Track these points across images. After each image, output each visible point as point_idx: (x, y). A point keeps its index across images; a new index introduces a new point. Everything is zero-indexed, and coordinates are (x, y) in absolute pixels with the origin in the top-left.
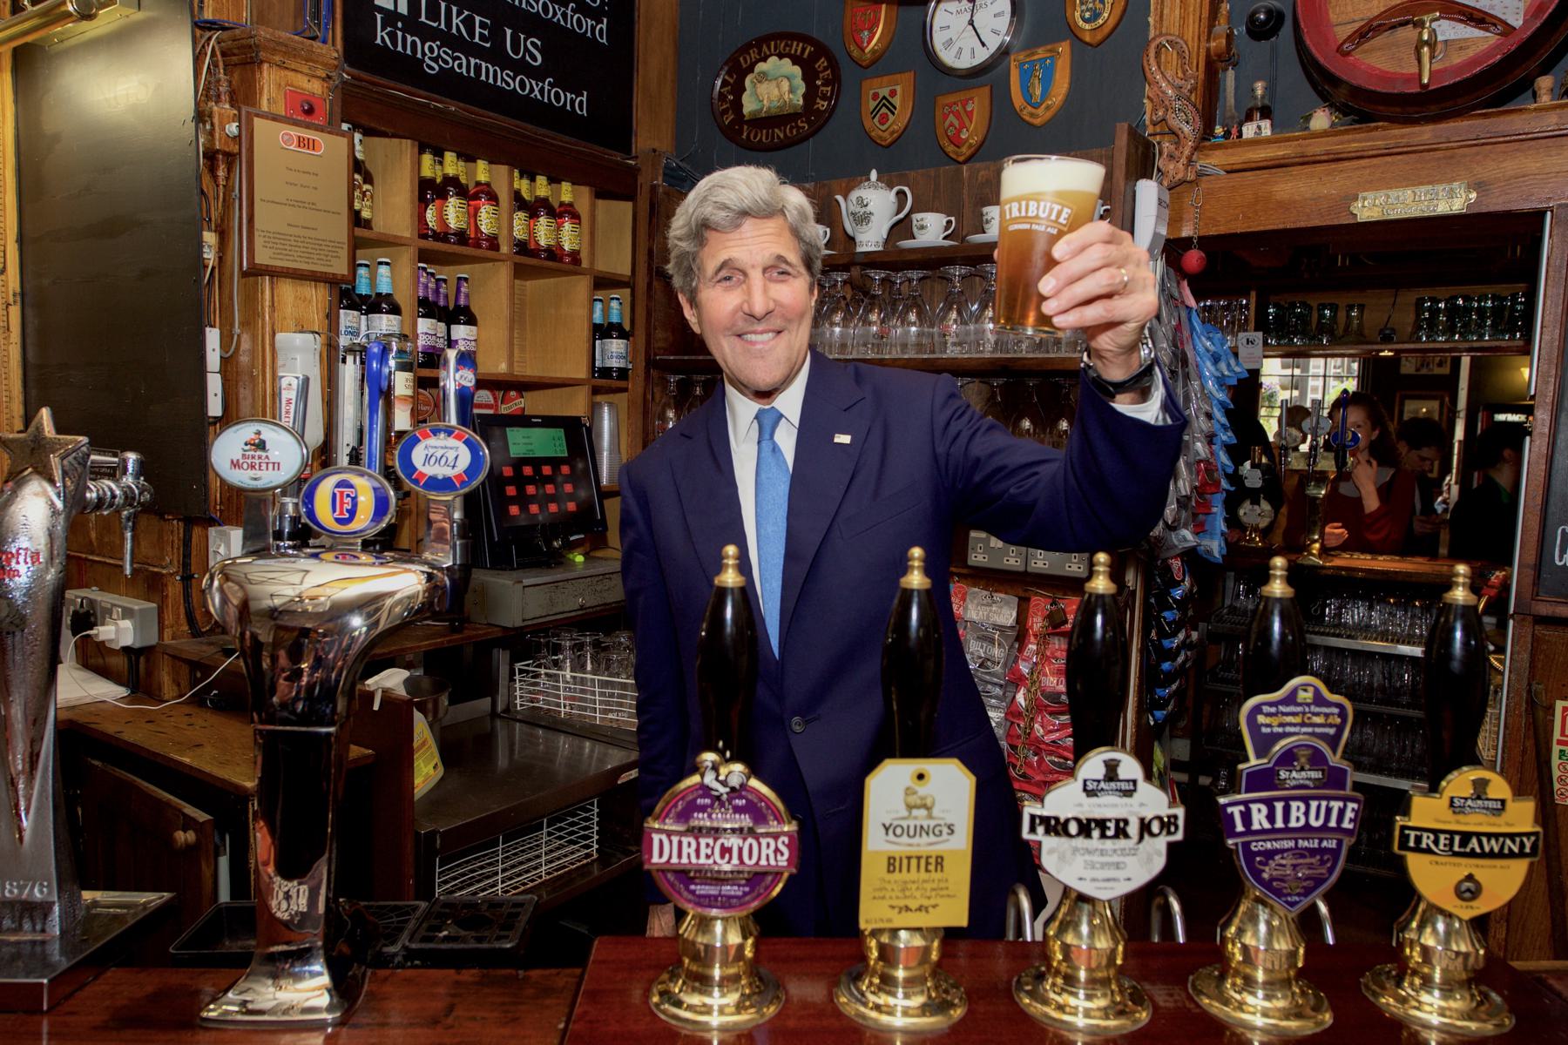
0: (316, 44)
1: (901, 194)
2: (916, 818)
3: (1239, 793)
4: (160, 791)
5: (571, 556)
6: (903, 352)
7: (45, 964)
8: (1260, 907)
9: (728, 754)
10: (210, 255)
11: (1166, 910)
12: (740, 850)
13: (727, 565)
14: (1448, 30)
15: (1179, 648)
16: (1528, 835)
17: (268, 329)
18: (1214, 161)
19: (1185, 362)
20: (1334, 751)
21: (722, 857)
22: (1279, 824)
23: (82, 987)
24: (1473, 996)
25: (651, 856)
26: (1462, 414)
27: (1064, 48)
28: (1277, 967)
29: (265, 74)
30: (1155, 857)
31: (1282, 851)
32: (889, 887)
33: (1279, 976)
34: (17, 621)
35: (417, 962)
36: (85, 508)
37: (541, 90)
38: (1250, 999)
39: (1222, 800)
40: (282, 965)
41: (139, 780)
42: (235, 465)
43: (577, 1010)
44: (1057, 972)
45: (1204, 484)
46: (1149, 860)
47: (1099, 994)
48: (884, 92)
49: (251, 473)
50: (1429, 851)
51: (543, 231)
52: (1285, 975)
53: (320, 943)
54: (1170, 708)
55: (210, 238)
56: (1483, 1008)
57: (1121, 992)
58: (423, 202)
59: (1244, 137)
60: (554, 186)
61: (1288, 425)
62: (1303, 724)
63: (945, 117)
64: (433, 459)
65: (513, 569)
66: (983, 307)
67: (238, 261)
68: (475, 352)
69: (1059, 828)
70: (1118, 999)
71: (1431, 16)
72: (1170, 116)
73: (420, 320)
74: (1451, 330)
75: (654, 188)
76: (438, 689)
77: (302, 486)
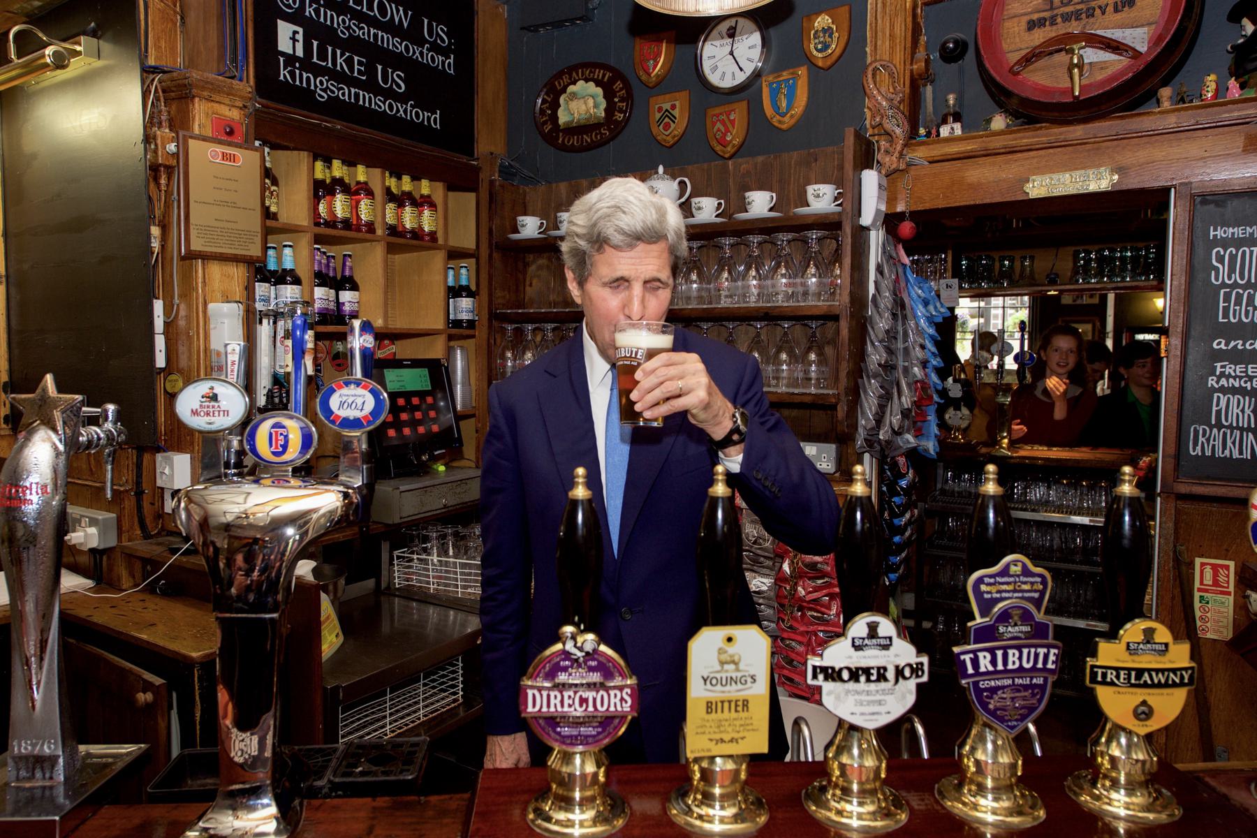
0: (235, 82)
1: (682, 184)
2: (727, 671)
3: (969, 644)
4: (123, 662)
5: (435, 467)
6: (688, 304)
7: (56, 808)
8: (987, 730)
9: (582, 627)
10: (156, 245)
11: (913, 731)
12: (595, 700)
13: (578, 483)
14: (1092, 55)
15: (906, 525)
16: (1186, 669)
17: (201, 300)
18: (919, 154)
19: (903, 306)
20: (1039, 610)
21: (581, 705)
22: (1000, 667)
23: (83, 822)
24: (1150, 794)
25: (526, 707)
26: (1111, 335)
27: (802, 71)
28: (1002, 776)
29: (197, 105)
30: (908, 695)
31: (1003, 687)
32: (708, 725)
33: (1004, 783)
34: (31, 539)
35: (340, 793)
36: (79, 449)
37: (406, 111)
38: (982, 801)
39: (956, 650)
40: (241, 799)
41: (106, 654)
42: (195, 413)
43: (472, 828)
44: (836, 786)
45: (920, 399)
46: (904, 697)
47: (868, 801)
48: (667, 106)
49: (207, 419)
50: (1112, 684)
51: (408, 218)
52: (1008, 782)
53: (268, 782)
54: (901, 571)
55: (155, 231)
56: (1158, 802)
57: (886, 799)
58: (317, 199)
59: (942, 135)
60: (415, 182)
61: (981, 348)
62: (1015, 591)
63: (714, 124)
64: (346, 405)
65: (391, 478)
66: (748, 269)
67: (177, 248)
68: (357, 312)
69: (835, 675)
70: (883, 805)
71: (1079, 45)
72: (885, 122)
73: (316, 288)
74: (1100, 274)
75: (492, 183)
76: (338, 574)
77: (246, 426)
